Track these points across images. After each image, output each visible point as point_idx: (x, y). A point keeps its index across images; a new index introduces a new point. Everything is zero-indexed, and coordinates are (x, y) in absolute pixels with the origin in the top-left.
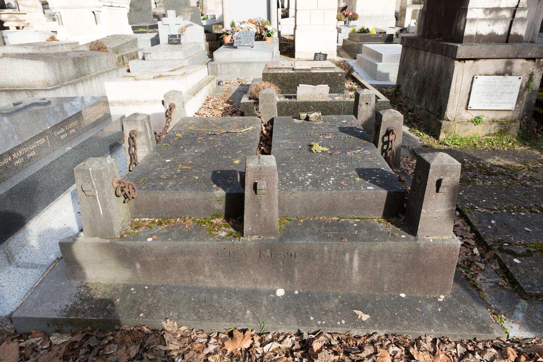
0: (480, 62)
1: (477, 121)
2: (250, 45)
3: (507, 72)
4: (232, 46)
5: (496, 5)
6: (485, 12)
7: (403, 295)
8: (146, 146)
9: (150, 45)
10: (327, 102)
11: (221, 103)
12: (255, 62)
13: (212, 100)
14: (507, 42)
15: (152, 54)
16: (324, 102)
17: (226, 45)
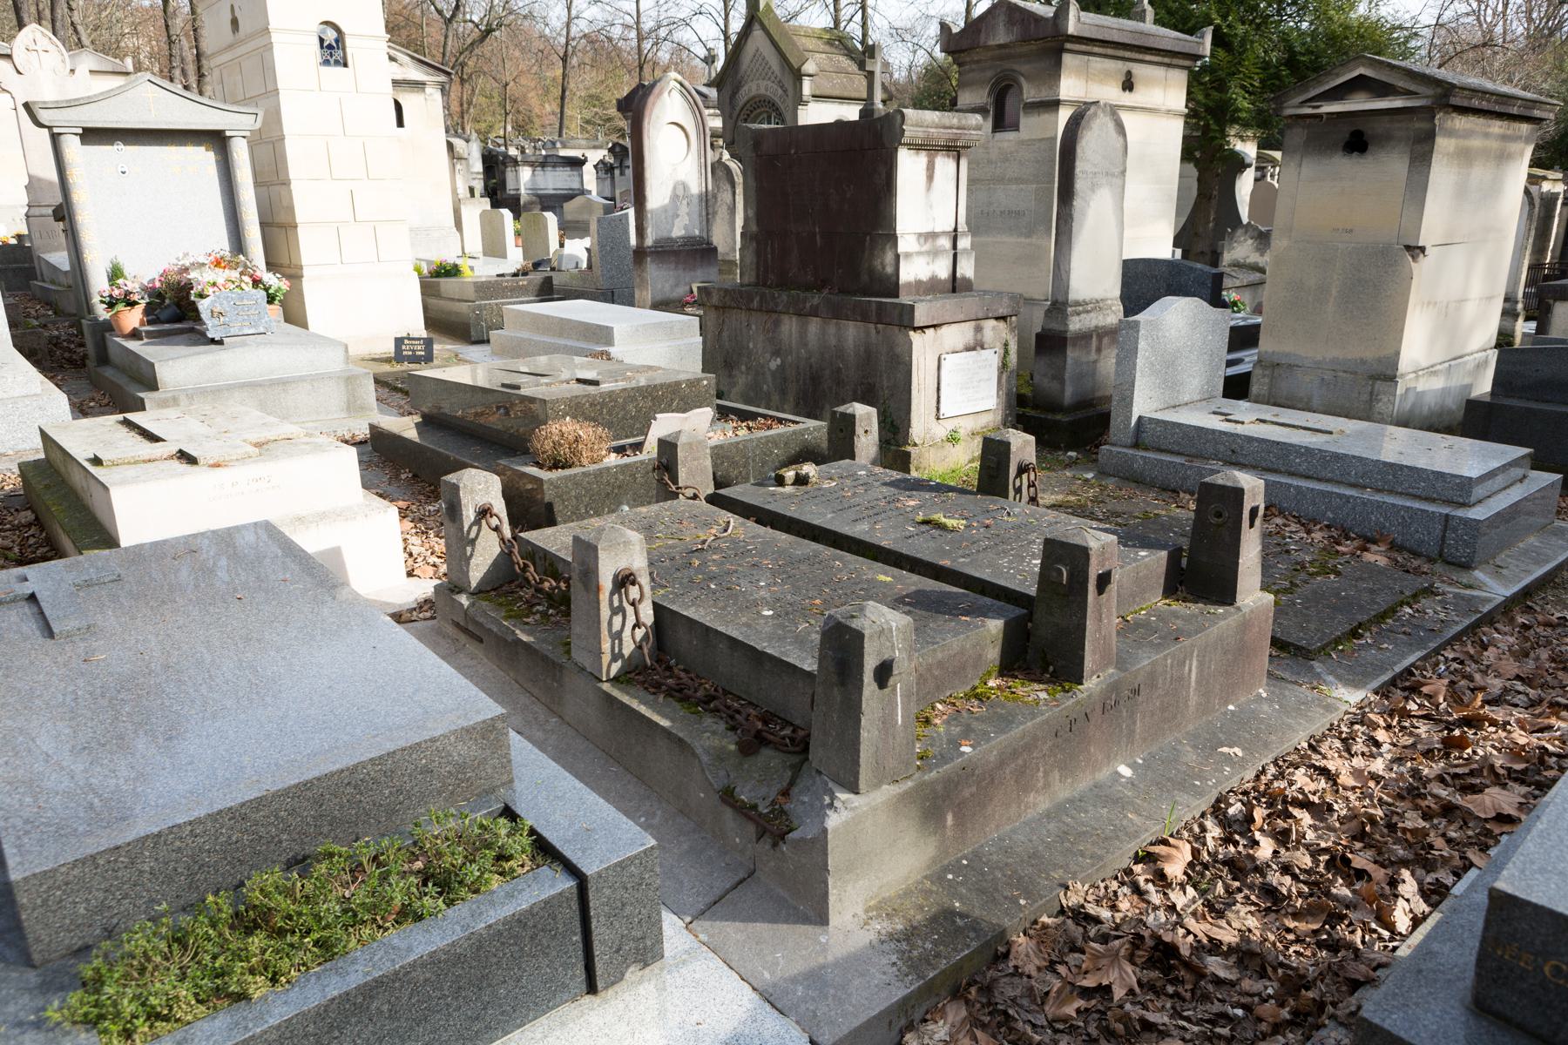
0: (945, 328)
1: (953, 439)
3: (977, 346)
5: (929, 229)
6: (918, 239)
7: (1231, 707)
12: (302, 379)
14: (954, 290)
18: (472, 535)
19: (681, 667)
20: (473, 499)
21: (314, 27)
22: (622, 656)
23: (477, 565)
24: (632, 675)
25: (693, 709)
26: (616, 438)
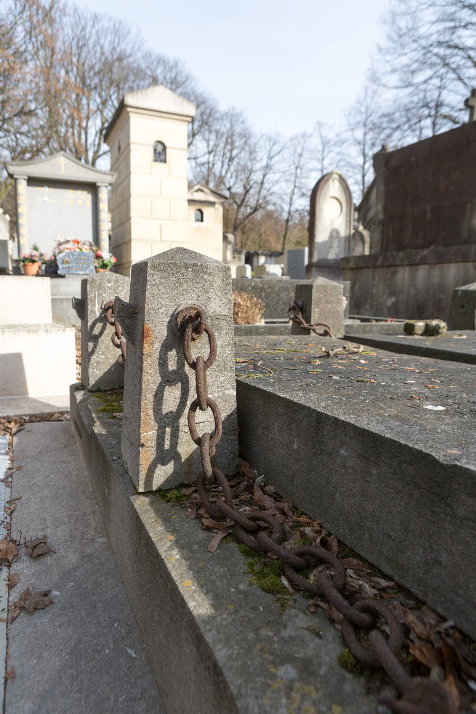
18: (96, 331)
19: (270, 489)
20: (100, 295)
21: (152, 142)
22: (176, 456)
23: (98, 363)
24: (185, 491)
25: (269, 581)
26: (270, 317)
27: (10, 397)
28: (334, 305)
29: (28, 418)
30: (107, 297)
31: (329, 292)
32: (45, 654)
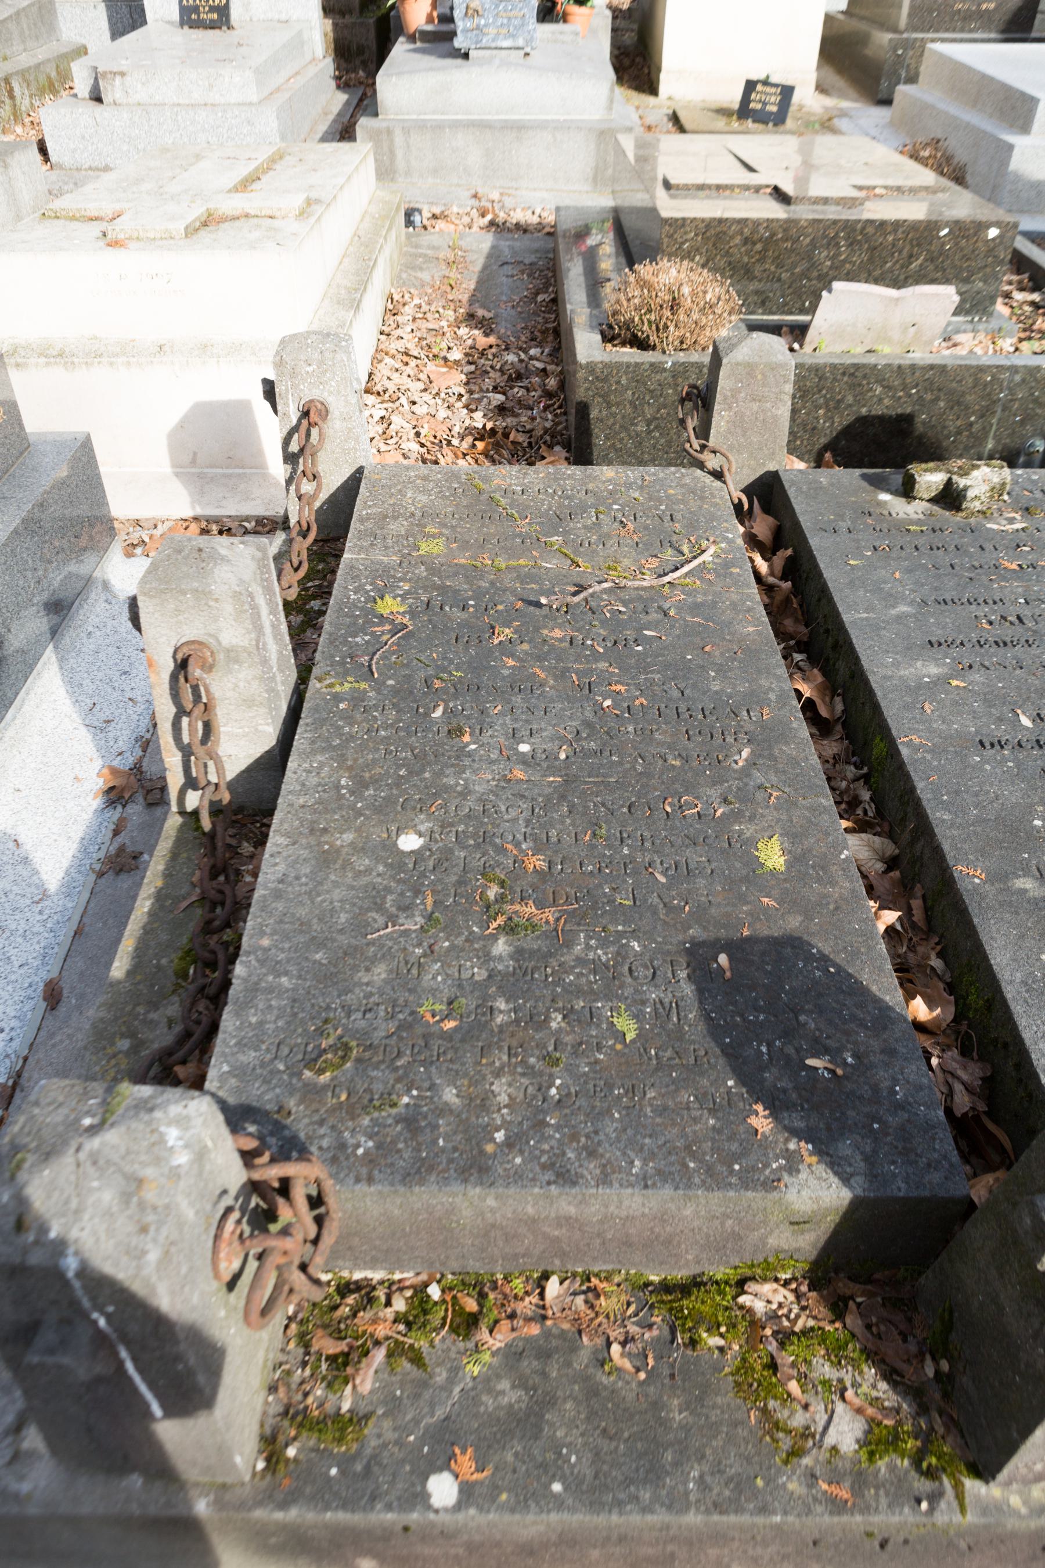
2: (520, 42)
4: (444, 46)
8: (263, 710)
9: (107, 34)
10: (945, 366)
11: (444, 323)
12: (542, 126)
13: (409, 310)
15: (128, 78)
16: (932, 367)
17: (412, 38)
27: (241, 471)
28: (768, 405)
29: (253, 523)
30: (306, 391)
31: (759, 377)
32: (110, 921)
